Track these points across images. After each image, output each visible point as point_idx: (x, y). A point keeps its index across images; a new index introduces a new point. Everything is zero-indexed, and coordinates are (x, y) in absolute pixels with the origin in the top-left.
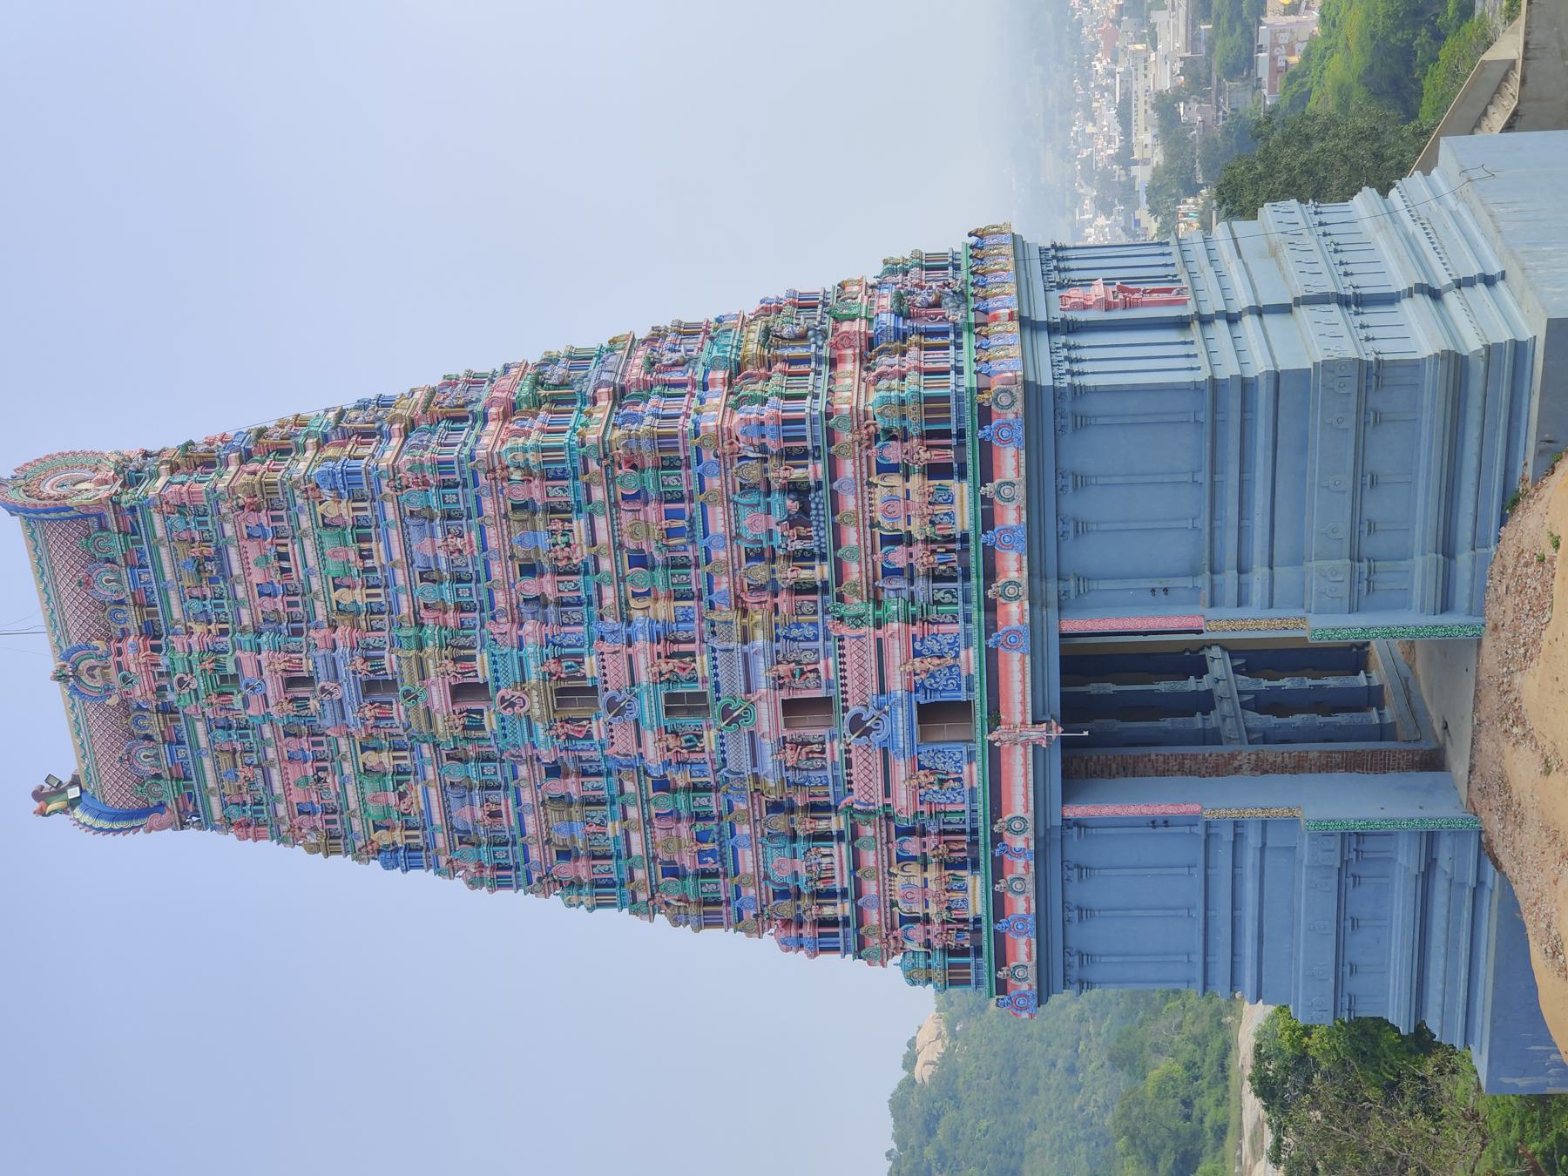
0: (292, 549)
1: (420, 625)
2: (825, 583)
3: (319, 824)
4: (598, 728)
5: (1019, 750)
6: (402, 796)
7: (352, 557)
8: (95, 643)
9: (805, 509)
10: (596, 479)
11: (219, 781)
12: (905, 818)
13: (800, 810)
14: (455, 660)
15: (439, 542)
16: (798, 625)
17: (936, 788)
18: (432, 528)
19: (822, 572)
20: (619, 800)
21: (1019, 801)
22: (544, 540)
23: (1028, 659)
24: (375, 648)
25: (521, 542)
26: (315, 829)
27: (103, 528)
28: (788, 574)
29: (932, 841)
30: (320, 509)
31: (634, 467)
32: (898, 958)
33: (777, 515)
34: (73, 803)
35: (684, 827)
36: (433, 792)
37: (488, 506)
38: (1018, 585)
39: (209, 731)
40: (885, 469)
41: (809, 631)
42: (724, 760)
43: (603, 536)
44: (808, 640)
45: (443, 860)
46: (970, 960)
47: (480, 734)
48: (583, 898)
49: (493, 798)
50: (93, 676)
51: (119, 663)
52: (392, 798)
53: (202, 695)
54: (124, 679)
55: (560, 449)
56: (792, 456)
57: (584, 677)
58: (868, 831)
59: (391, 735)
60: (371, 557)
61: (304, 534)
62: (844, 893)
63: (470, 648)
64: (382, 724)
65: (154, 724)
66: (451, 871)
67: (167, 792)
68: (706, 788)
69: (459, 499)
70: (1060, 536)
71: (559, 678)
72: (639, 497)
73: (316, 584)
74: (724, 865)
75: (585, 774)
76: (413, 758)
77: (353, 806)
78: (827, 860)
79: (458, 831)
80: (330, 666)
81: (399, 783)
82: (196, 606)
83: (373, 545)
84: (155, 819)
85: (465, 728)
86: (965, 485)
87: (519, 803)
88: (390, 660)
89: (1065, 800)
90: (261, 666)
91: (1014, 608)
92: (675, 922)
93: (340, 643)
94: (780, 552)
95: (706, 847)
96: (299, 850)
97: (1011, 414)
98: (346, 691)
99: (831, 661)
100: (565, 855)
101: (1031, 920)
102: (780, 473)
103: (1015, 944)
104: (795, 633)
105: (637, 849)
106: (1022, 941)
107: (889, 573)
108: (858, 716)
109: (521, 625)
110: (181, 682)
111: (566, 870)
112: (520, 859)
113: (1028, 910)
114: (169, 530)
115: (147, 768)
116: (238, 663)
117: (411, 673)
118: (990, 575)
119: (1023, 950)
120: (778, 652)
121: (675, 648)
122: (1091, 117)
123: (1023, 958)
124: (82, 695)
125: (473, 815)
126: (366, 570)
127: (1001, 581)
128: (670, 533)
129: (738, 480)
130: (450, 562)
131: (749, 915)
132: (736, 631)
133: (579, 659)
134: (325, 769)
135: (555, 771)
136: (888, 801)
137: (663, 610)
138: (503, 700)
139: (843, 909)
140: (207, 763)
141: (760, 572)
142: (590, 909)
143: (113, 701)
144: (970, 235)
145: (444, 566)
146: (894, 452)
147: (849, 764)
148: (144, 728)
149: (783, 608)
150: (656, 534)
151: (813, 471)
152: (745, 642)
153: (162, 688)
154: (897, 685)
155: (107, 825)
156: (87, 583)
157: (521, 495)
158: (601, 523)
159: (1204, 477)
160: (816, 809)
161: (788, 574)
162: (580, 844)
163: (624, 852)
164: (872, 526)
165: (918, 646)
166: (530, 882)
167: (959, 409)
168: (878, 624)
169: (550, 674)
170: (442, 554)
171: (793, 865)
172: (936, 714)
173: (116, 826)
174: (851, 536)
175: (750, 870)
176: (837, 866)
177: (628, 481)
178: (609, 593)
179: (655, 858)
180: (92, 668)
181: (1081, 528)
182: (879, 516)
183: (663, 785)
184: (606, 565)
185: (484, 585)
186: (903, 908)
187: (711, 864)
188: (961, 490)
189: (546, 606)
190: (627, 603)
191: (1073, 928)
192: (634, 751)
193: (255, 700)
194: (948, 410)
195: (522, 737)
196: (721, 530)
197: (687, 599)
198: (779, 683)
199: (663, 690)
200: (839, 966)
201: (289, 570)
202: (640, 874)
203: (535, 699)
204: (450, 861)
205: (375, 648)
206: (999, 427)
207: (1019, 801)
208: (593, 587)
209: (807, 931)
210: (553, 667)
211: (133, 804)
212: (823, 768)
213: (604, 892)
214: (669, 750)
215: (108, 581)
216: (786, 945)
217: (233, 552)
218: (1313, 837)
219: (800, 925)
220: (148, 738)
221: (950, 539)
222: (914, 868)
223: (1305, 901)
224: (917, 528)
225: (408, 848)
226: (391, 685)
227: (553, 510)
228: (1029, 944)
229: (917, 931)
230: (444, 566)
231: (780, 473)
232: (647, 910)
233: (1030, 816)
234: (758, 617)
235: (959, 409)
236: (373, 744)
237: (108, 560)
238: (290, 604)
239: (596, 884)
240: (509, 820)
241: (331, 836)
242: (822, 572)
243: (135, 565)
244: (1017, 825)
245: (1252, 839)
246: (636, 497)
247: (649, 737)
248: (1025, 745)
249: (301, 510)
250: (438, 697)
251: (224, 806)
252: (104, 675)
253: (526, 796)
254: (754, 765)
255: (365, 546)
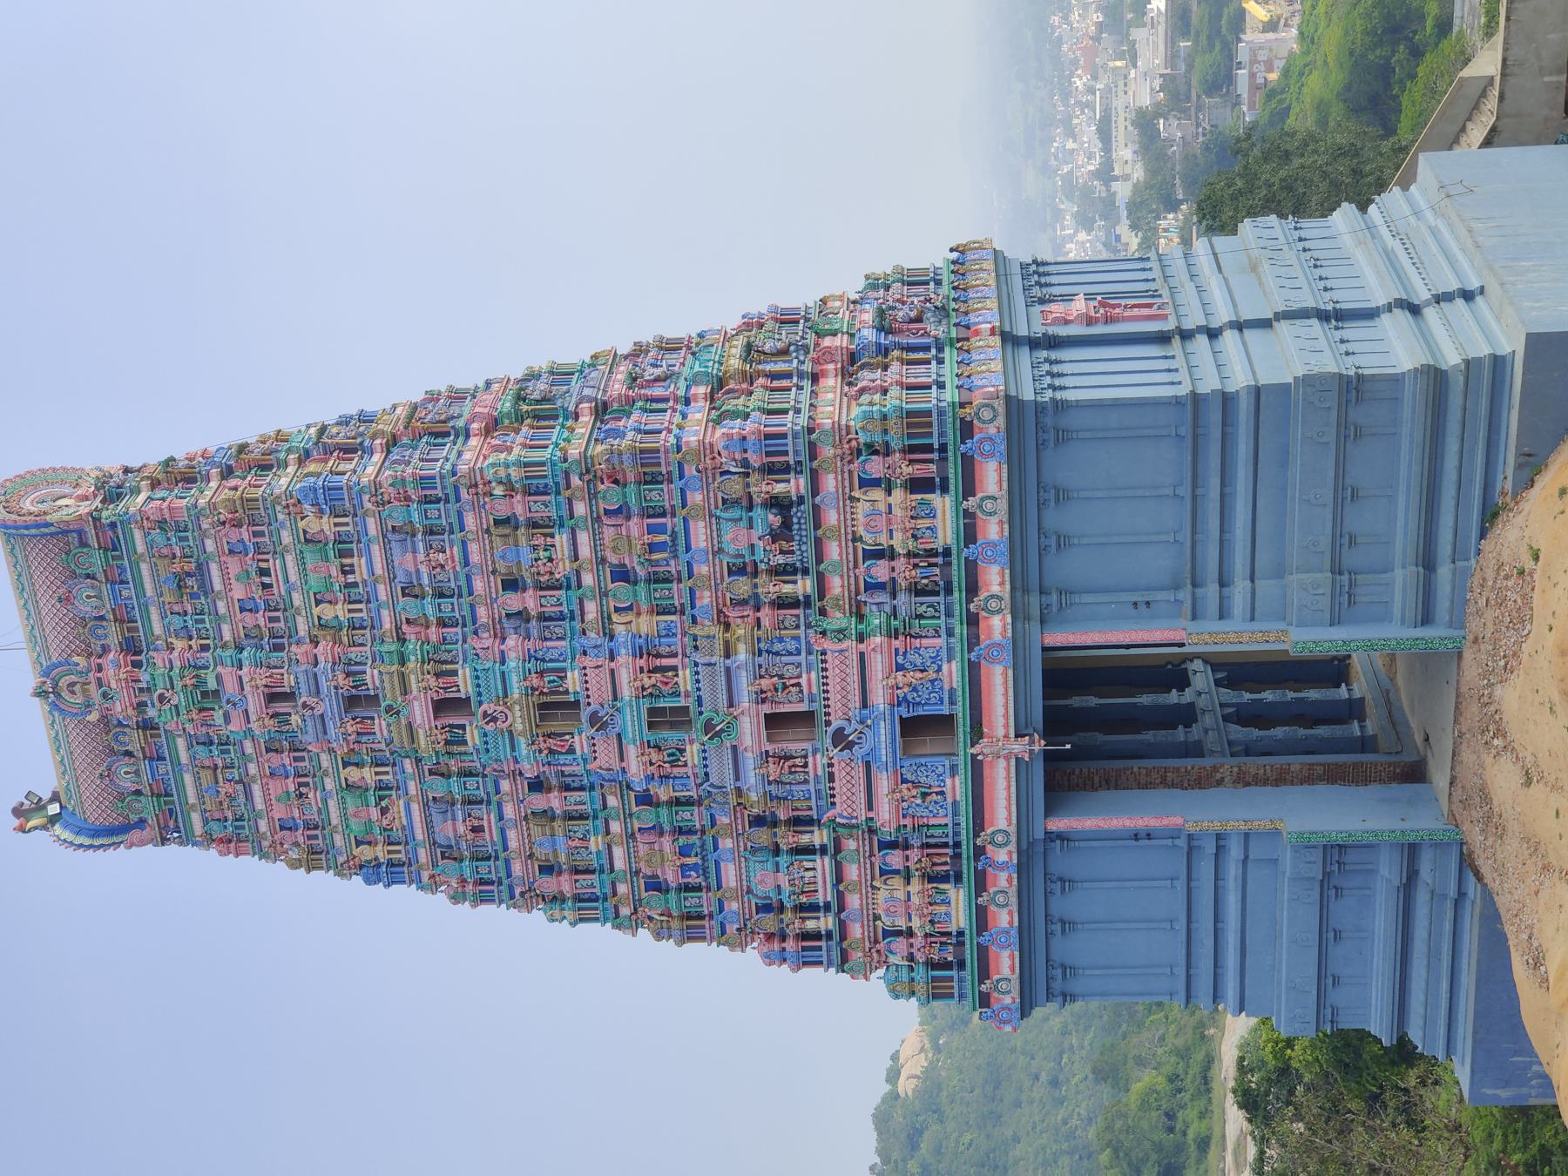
0: (274, 564)
1: (402, 640)
2: (807, 597)
3: (301, 840)
4: (580, 743)
5: (1002, 763)
6: (384, 811)
7: (334, 572)
8: (76, 659)
9: (787, 524)
10: (578, 494)
11: (200, 797)
12: (888, 831)
13: (782, 824)
14: (437, 675)
15: (421, 557)
16: (781, 640)
17: (919, 801)
18: (413, 543)
19: (804, 586)
20: (601, 815)
21: (1002, 814)
22: (527, 556)
23: (1010, 673)
24: (357, 664)
25: (503, 557)
26: (296, 844)
27: (83, 544)
28: (770, 588)
29: (914, 854)
30: (301, 524)
31: (616, 482)
32: (881, 972)
33: (759, 529)
34: (53, 820)
35: (667, 843)
36: (415, 807)
37: (470, 520)
38: (1000, 599)
39: (190, 747)
40: (868, 483)
41: (792, 646)
42: (706, 774)
43: (585, 551)
44: (790, 654)
45: (425, 875)
46: (954, 973)
47: (462, 749)
48: (566, 913)
49: (475, 813)
50: (73, 693)
51: (99, 679)
52: (375, 813)
53: (183, 711)
54: (105, 695)
55: (542, 464)
56: (769, 470)
57: (567, 692)
58: (851, 845)
59: (373, 750)
60: (353, 572)
61: (286, 550)
62: (827, 907)
63: (452, 662)
64: (364, 739)
65: (134, 741)
66: (433, 886)
67: (148, 808)
68: (689, 802)
69: (441, 515)
70: (1042, 551)
71: (542, 693)
72: (622, 512)
73: (297, 599)
74: (706, 878)
75: (568, 788)
76: (395, 774)
77: (335, 822)
78: (811, 873)
79: (440, 846)
80: (312, 682)
81: (381, 798)
82: (177, 622)
83: (355, 560)
84: (135, 835)
85: (447, 742)
86: (947, 499)
87: (501, 818)
88: (372, 676)
89: (1049, 811)
90: (243, 681)
91: (996, 621)
92: (658, 936)
93: (321, 659)
94: (763, 566)
95: (691, 861)
96: (281, 865)
97: (993, 428)
98: (328, 706)
99: (813, 675)
100: (547, 869)
101: (1014, 933)
102: (762, 488)
103: (998, 956)
104: (777, 647)
105: (619, 864)
106: (1005, 954)
107: (871, 587)
108: (841, 730)
109: (504, 639)
110: (161, 698)
111: (548, 884)
112: (503, 874)
113: (1011, 923)
114: (150, 546)
115: (127, 784)
116: (219, 678)
117: (393, 688)
118: (972, 589)
119: (1006, 963)
120: (760, 666)
121: (658, 662)
122: (1071, 133)
123: (1006, 971)
124: (61, 711)
125: (455, 830)
126: (348, 585)
127: (983, 595)
128: (652, 548)
129: (720, 495)
130: (432, 577)
131: (732, 928)
132: (719, 647)
133: (561, 673)
134: (307, 785)
135: (537, 785)
136: (871, 815)
137: (646, 624)
138: (485, 714)
139: (826, 922)
140: (188, 779)
141: (743, 586)
142: (573, 924)
143: (93, 717)
144: (952, 250)
145: (426, 581)
146: (876, 467)
147: (831, 778)
148: (125, 744)
149: (766, 622)
150: (638, 549)
151: (794, 486)
152: (727, 656)
153: (142, 704)
154: (879, 698)
155: (87, 842)
156: (67, 599)
157: (502, 510)
158: (583, 538)
159: (1185, 491)
160: (798, 823)
161: (770, 588)
162: (563, 858)
163: (607, 867)
164: (854, 540)
165: (900, 660)
166: (512, 897)
167: (941, 424)
168: (861, 638)
169: (533, 689)
170: (424, 569)
171: (776, 879)
172: (919, 727)
173: (97, 842)
174: (833, 550)
175: (733, 884)
176: (820, 880)
177: (611, 496)
178: (591, 608)
179: (637, 872)
180: (73, 684)
181: (1063, 542)
182: (861, 531)
183: (646, 799)
184: (588, 579)
185: (466, 600)
186: (887, 921)
187: (694, 878)
188: (944, 505)
189: (528, 621)
190: (609, 618)
191: (1056, 942)
192: (616, 766)
193: (236, 716)
194: (930, 425)
195: (505, 752)
196: (703, 545)
197: (669, 613)
198: (761, 697)
199: (646, 704)
200: (822, 980)
201: (270, 586)
202: (622, 889)
203: (518, 714)
204: (432, 877)
205: (357, 664)
206: (981, 441)
207: (1002, 814)
208: (575, 601)
209: (790, 945)
210: (535, 682)
211: (114, 820)
212: (806, 782)
213: (586, 906)
214: (651, 764)
215: (89, 597)
216: (769, 959)
217: (214, 568)
218: (1296, 849)
219: (783, 938)
220: (129, 754)
221: (932, 553)
222: (897, 882)
223: (1287, 913)
224: (899, 542)
225: (391, 864)
226: (373, 700)
227: (535, 525)
228: (1012, 957)
229: (900, 944)
230: (426, 581)
231: (762, 488)
232: (631, 924)
233: (1013, 829)
234: (741, 632)
235: (941, 424)
236: (355, 759)
237: (88, 576)
238: (272, 620)
239: (578, 898)
240: (491, 835)
241: (313, 851)
242: (804, 586)
243: (116, 580)
244: (993, 604)
245: (1235, 851)
246: (618, 511)
247: (632, 752)
248: (1007, 758)
249: (282, 525)
250: (420, 711)
251: (206, 822)
252: (85, 691)
253: (509, 811)
254: (737, 779)
255: (347, 561)
